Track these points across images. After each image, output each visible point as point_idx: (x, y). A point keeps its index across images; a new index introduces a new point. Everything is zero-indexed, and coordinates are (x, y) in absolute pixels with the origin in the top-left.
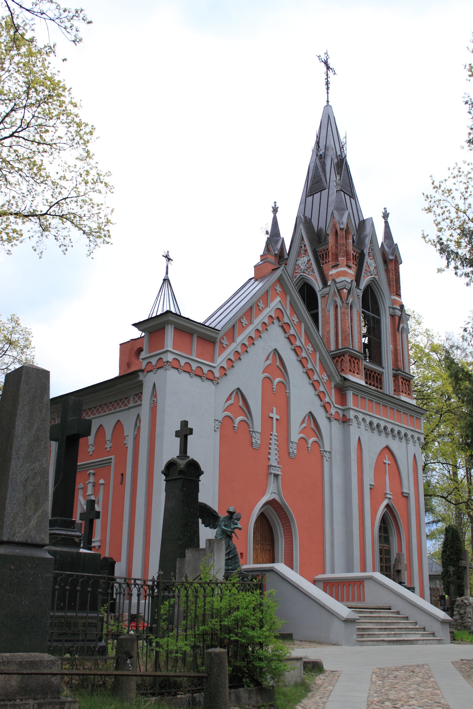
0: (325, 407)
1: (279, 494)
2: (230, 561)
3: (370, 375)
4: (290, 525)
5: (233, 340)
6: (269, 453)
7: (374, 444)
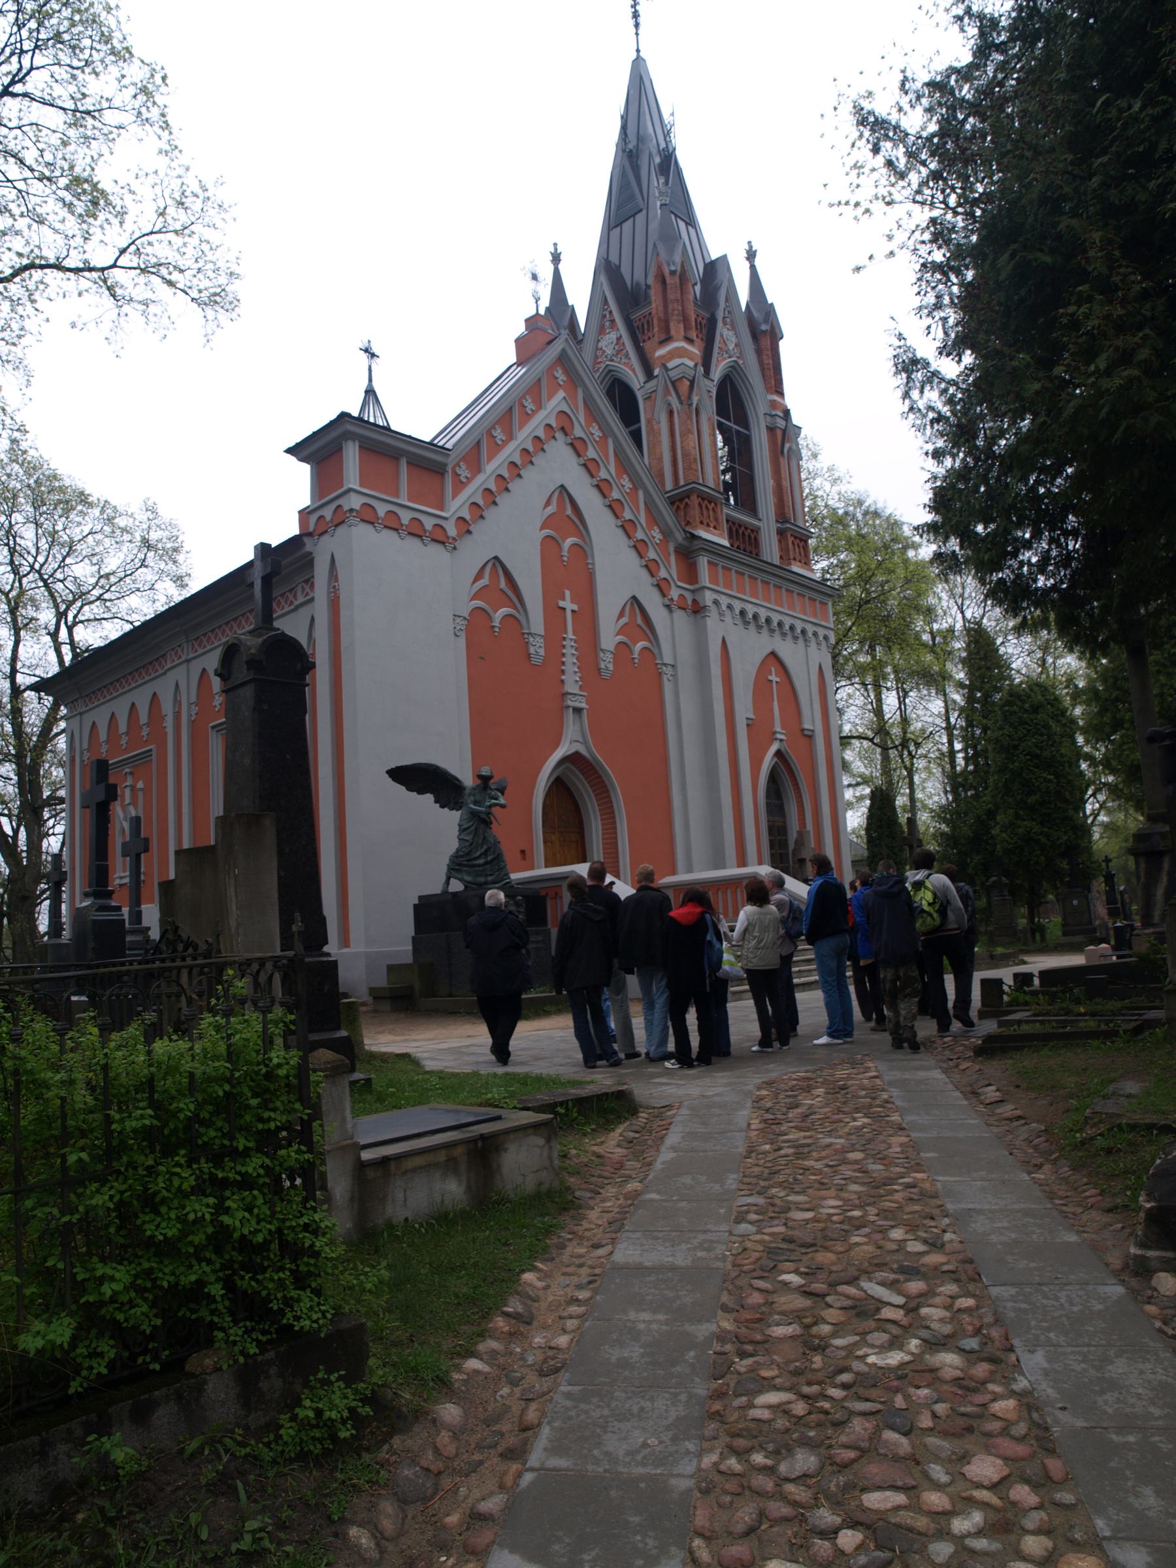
0: (662, 587)
2: (488, 866)
3: (737, 531)
4: (609, 796)
5: (477, 468)
6: (563, 672)
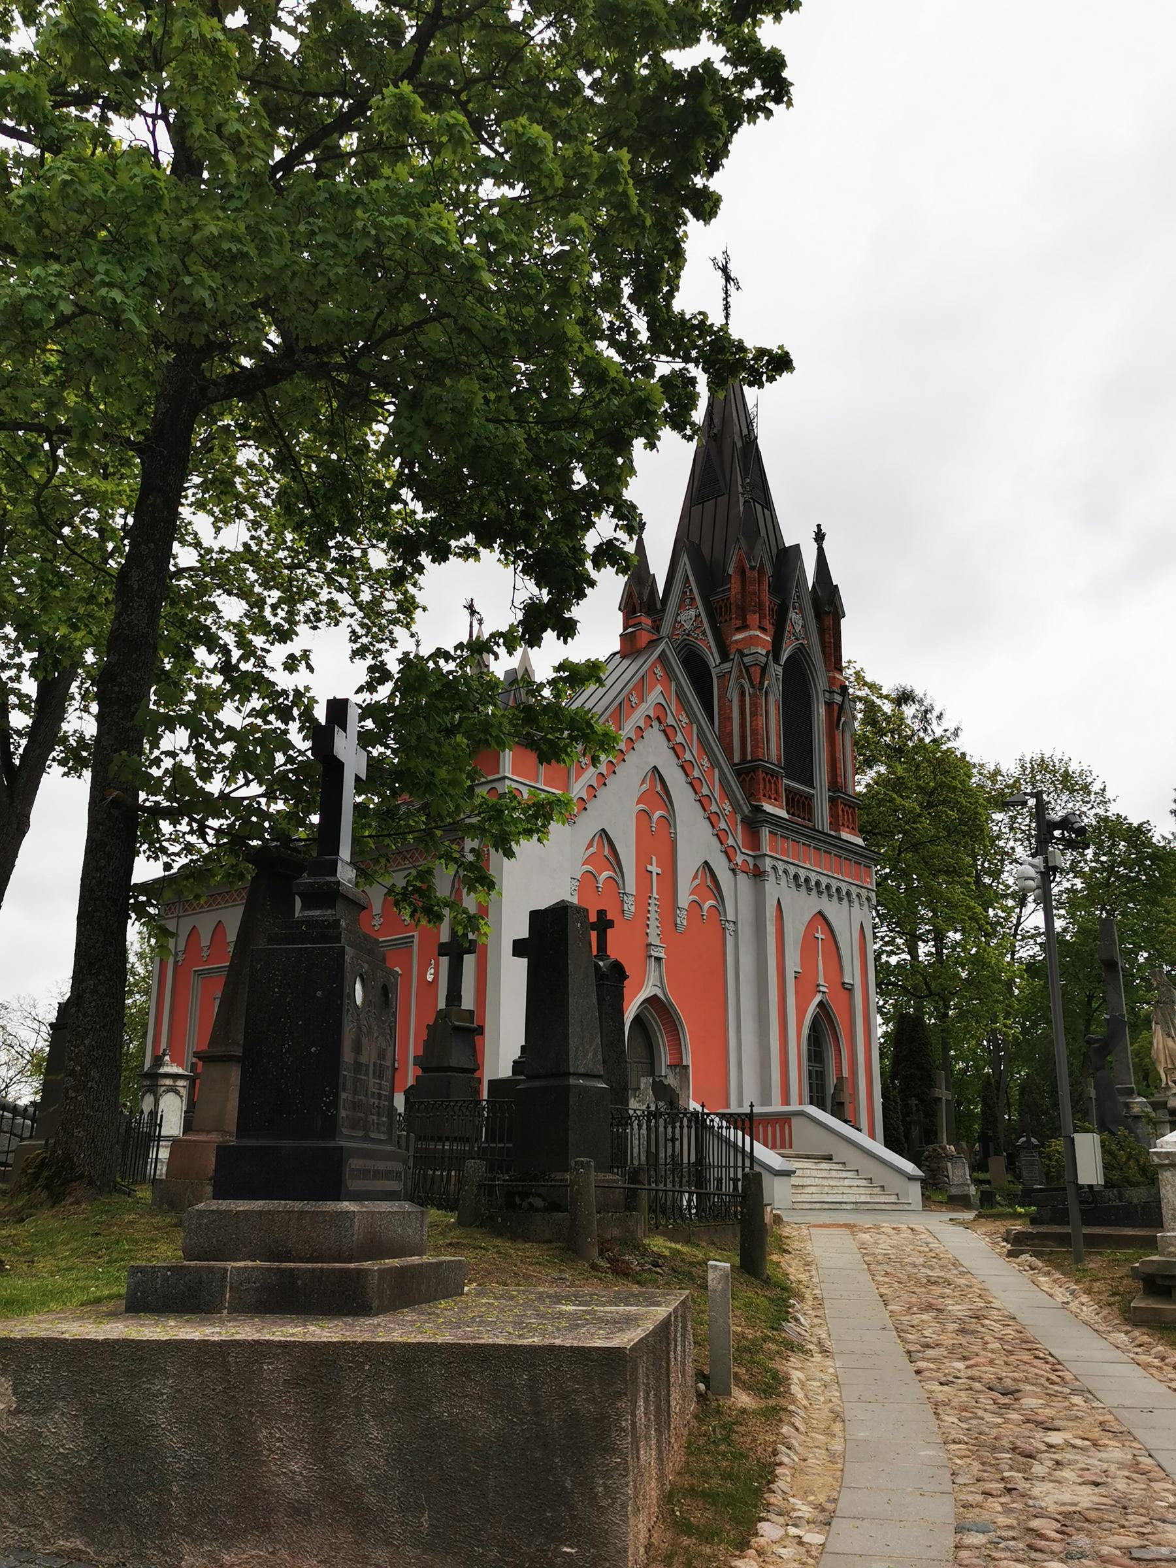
0: (728, 854)
1: (662, 987)
3: (793, 799)
7: (800, 909)
